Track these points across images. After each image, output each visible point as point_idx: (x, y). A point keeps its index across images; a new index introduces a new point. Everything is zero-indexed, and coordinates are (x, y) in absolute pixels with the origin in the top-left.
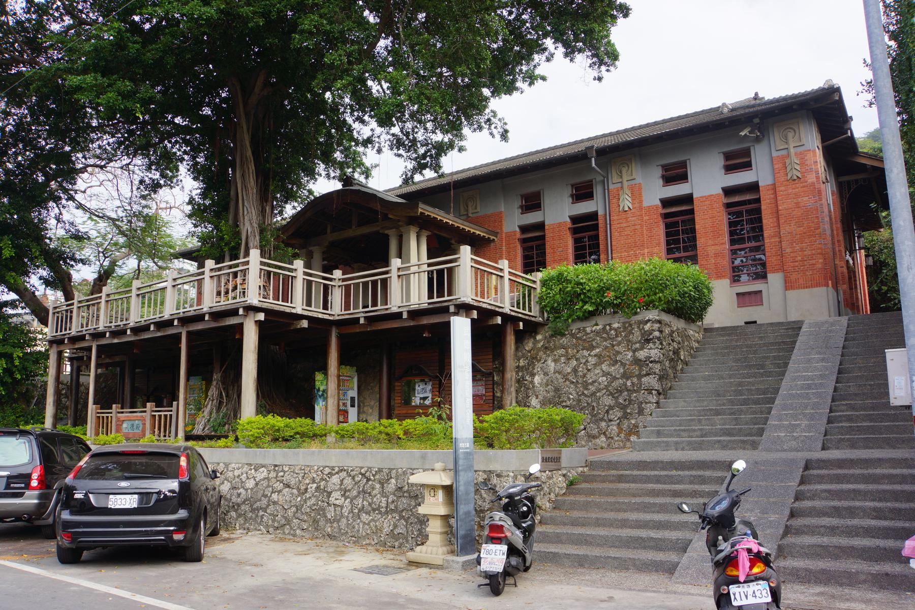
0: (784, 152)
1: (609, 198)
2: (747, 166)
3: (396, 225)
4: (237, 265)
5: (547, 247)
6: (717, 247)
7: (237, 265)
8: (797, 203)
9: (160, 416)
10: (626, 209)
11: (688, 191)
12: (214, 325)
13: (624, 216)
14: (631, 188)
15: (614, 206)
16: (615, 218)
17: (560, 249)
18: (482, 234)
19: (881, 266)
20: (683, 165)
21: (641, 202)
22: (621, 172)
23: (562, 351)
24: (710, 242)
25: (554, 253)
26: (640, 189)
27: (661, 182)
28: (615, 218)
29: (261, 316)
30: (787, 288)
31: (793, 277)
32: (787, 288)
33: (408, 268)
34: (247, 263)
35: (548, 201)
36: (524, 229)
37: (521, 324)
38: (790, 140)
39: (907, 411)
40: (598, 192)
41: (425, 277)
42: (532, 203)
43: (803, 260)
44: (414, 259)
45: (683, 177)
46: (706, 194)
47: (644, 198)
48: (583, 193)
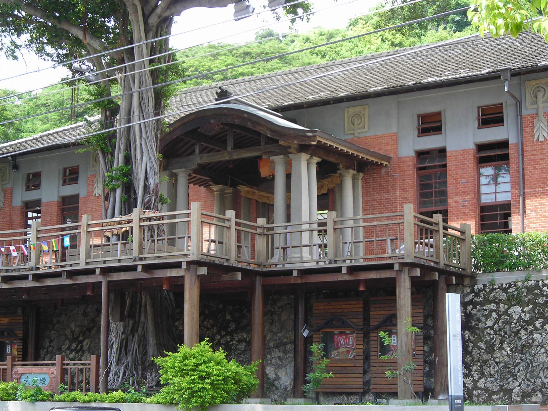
1: (524, 125)
3: (285, 151)
4: (174, 217)
5: (449, 177)
7: (174, 217)
12: (145, 276)
13: (540, 147)
15: (527, 135)
16: (529, 148)
17: (464, 180)
18: (351, 152)
19: (455, 22)
23: (493, 306)
25: (457, 183)
28: (529, 148)
29: (203, 271)
33: (342, 222)
34: (188, 215)
36: (421, 155)
37: (454, 278)
39: (442, 169)
40: (509, 115)
42: (430, 125)
44: (349, 211)
48: (491, 117)
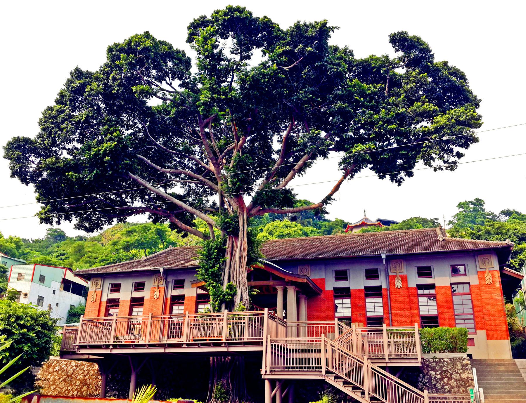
0: (484, 270)
2: (376, 277)
6: (449, 314)
8: (491, 296)
9: (287, 365)
10: (399, 287)
11: (379, 285)
14: (402, 276)
16: (393, 291)
20: (429, 268)
21: (407, 285)
22: (485, 263)
24: (446, 311)
26: (406, 278)
27: (334, 279)
30: (488, 339)
31: (491, 333)
32: (488, 339)
35: (351, 275)
38: (487, 264)
41: (127, 323)
42: (116, 288)
43: (495, 325)
45: (118, 290)
46: (443, 285)
47: (326, 286)
